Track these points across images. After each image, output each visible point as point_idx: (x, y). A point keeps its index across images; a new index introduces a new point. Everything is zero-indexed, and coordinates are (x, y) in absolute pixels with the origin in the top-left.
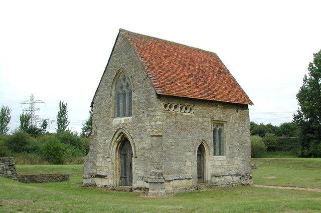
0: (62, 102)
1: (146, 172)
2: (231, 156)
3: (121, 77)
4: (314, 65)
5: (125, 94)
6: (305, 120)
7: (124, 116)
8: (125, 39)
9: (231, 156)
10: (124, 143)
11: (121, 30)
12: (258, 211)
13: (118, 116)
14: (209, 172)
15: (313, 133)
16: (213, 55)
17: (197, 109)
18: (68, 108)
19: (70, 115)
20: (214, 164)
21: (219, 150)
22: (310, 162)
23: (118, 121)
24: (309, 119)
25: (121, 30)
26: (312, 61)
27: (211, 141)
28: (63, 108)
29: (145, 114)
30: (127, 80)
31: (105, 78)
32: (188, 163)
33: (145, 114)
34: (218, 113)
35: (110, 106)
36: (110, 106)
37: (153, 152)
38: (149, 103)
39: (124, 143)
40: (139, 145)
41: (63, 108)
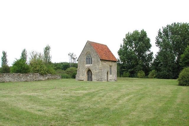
0: (4, 51)
1: (97, 78)
2: (113, 75)
3: (88, 54)
4: (126, 39)
5: (89, 58)
6: (121, 63)
7: (89, 64)
8: (89, 44)
9: (113, 75)
10: (89, 71)
11: (88, 41)
12: (28, 125)
13: (87, 64)
14: (109, 78)
15: (124, 68)
16: (106, 46)
17: (107, 62)
18: (7, 54)
19: (8, 58)
20: (110, 76)
21: (111, 74)
22: (128, 79)
23: (87, 65)
24: (123, 62)
25: (88, 41)
26: (125, 37)
27: (109, 71)
28: (4, 54)
29: (97, 64)
30: (90, 55)
31: (82, 53)
32: (105, 76)
33: (97, 64)
34: (110, 63)
35: (84, 61)
36: (84, 61)
37: (100, 73)
38: (98, 61)
39: (89, 71)
40: (93, 72)
41: (4, 54)
